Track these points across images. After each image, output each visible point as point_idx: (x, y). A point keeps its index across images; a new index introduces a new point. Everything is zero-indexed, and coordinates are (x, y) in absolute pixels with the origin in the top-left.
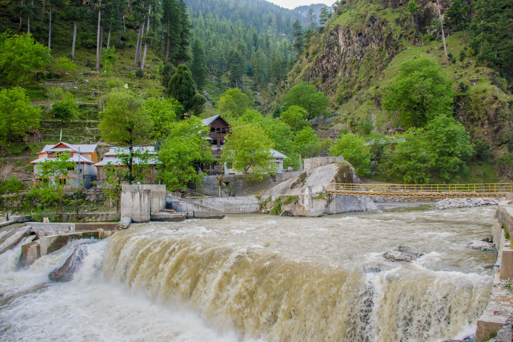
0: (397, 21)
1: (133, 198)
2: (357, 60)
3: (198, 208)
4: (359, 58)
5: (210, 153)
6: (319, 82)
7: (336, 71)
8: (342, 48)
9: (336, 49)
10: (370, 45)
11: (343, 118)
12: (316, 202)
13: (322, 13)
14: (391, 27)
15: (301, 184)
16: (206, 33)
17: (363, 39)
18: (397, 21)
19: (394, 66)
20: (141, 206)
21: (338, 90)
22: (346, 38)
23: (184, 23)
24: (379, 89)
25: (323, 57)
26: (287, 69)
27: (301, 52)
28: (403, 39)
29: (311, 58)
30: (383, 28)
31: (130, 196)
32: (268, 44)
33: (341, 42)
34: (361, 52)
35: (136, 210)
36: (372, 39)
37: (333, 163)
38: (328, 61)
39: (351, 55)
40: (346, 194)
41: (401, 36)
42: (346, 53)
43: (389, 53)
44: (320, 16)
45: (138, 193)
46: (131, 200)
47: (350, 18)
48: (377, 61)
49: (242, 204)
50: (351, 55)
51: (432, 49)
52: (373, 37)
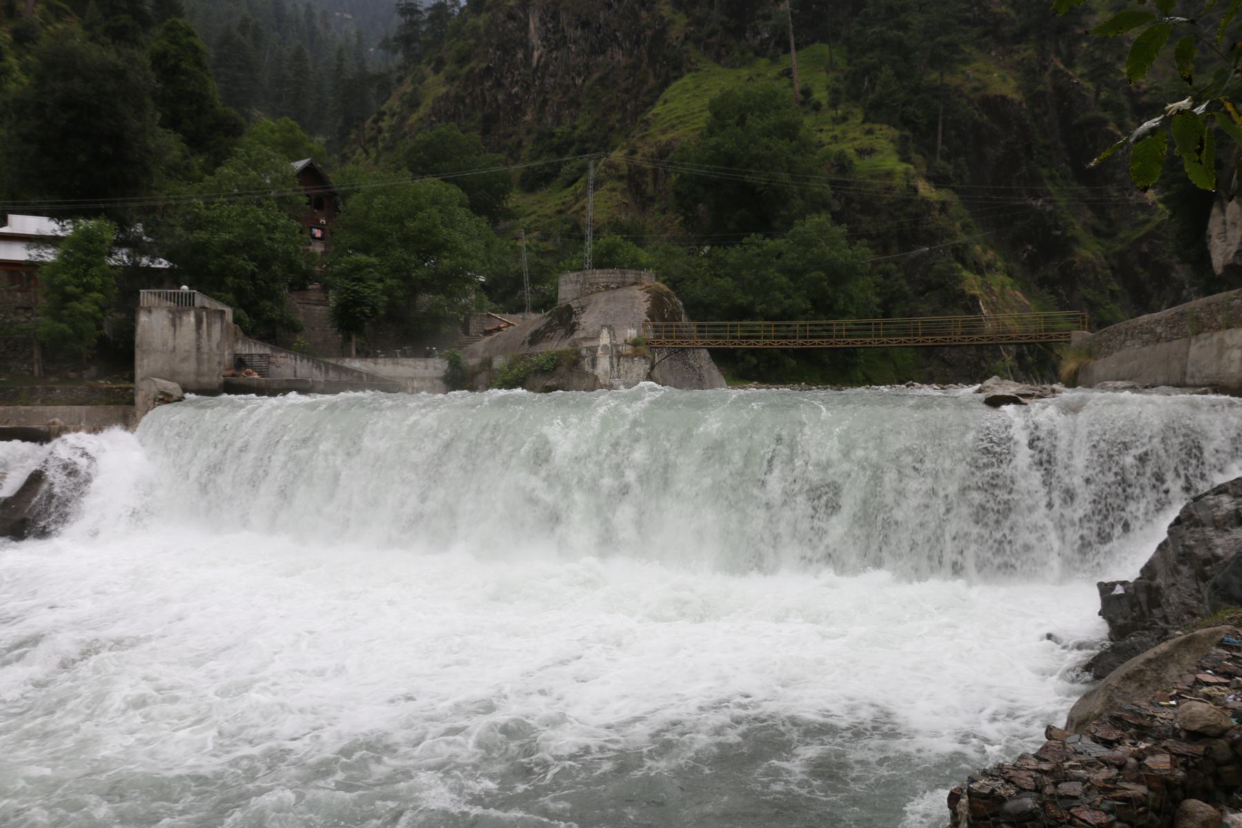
1: (174, 325)
2: (575, 85)
3: (327, 372)
4: (579, 81)
8: (536, 54)
9: (520, 55)
10: (609, 53)
14: (664, 14)
19: (670, 105)
20: (199, 349)
21: (524, 153)
22: (548, 30)
24: (638, 157)
25: (488, 70)
28: (690, 46)
30: (644, 14)
31: (166, 323)
33: (534, 39)
34: (587, 66)
37: (636, 284)
38: (499, 84)
39: (560, 73)
41: (687, 38)
42: (546, 66)
43: (657, 76)
45: (192, 314)
46: (168, 332)
48: (627, 91)
49: (412, 379)
50: (560, 73)
51: (759, 75)
52: (618, 34)
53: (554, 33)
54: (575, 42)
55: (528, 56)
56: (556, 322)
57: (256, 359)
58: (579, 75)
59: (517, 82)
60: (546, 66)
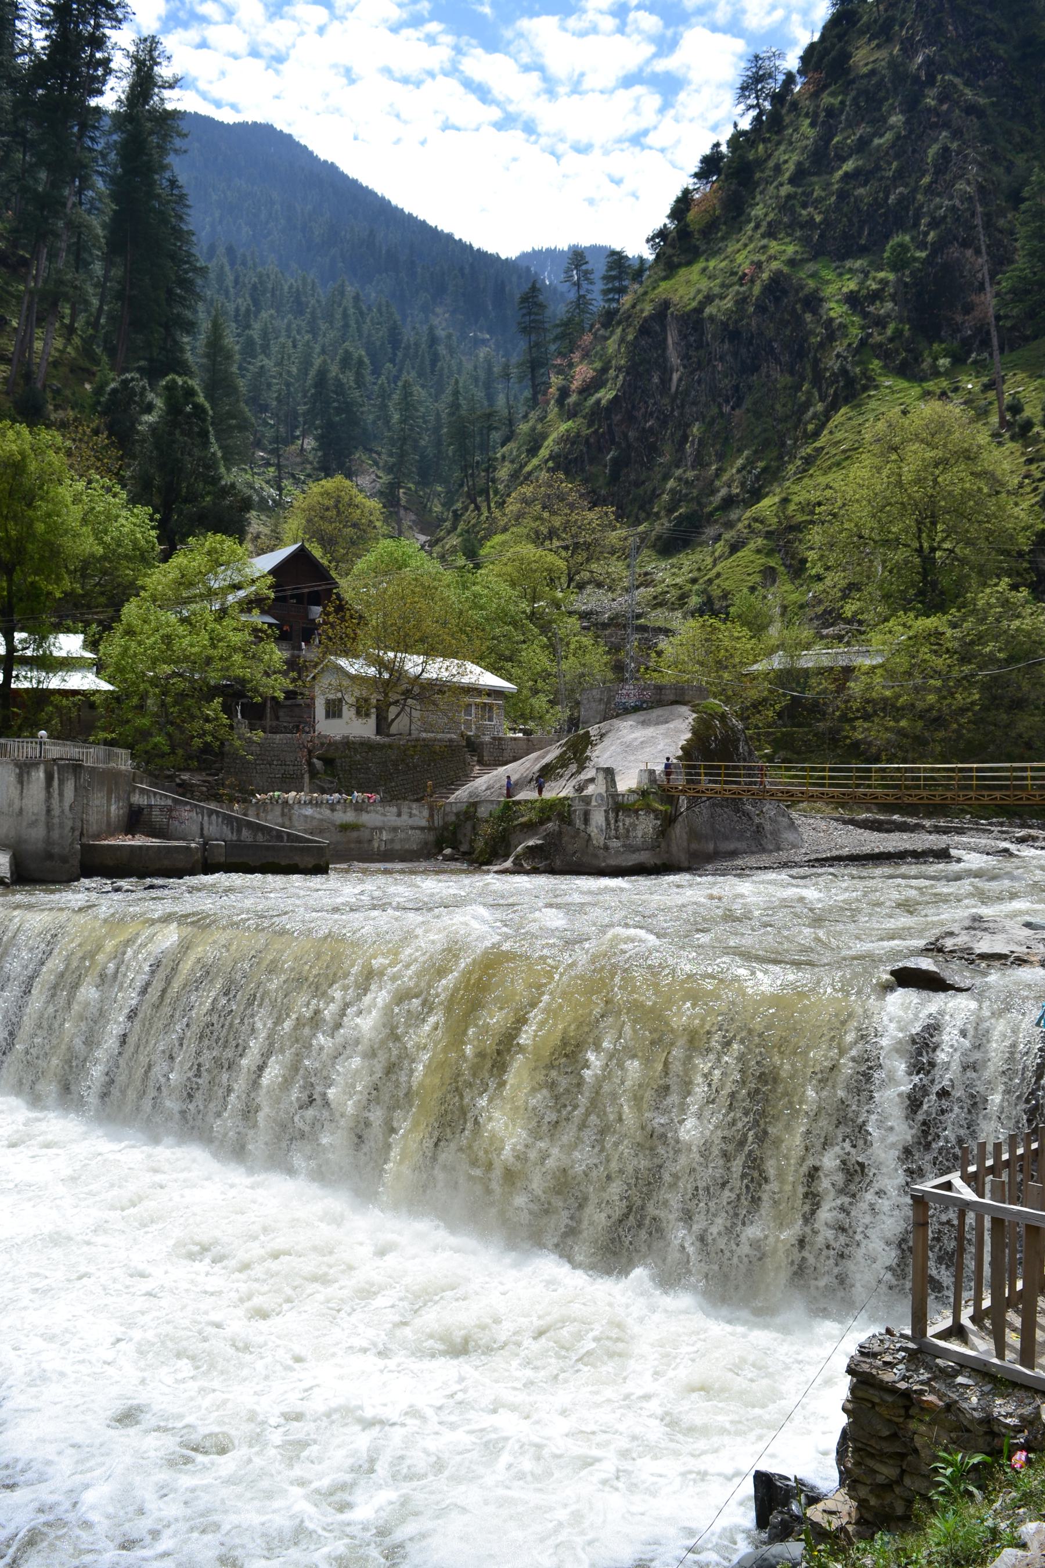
0: (853, 300)
1: (21, 782)
5: (268, 667)
6: (601, 481)
7: (654, 450)
8: (675, 377)
9: (656, 380)
11: (674, 593)
12: (628, 821)
13: (611, 268)
15: (573, 768)
16: (237, 310)
17: (743, 351)
18: (853, 300)
20: (49, 811)
22: (689, 346)
23: (180, 258)
24: (792, 507)
26: (496, 436)
27: (538, 389)
29: (577, 404)
32: (435, 359)
33: (674, 359)
35: (33, 824)
36: (772, 349)
38: (630, 418)
40: (728, 795)
42: (687, 393)
44: (604, 278)
45: (42, 768)
46: (14, 791)
47: (704, 284)
48: (786, 418)
49: (381, 829)
53: (697, 349)
54: (721, 359)
55: (665, 381)
56: (570, 754)
57: (156, 812)
58: (727, 402)
59: (651, 414)
60: (687, 393)
